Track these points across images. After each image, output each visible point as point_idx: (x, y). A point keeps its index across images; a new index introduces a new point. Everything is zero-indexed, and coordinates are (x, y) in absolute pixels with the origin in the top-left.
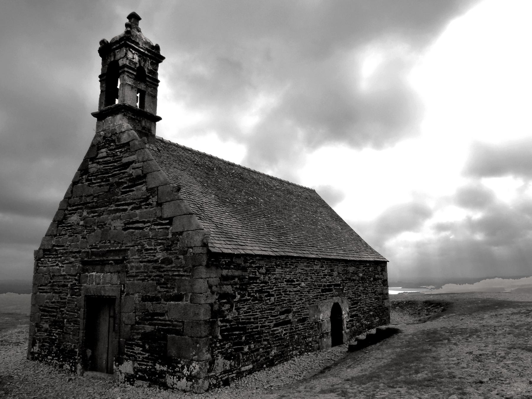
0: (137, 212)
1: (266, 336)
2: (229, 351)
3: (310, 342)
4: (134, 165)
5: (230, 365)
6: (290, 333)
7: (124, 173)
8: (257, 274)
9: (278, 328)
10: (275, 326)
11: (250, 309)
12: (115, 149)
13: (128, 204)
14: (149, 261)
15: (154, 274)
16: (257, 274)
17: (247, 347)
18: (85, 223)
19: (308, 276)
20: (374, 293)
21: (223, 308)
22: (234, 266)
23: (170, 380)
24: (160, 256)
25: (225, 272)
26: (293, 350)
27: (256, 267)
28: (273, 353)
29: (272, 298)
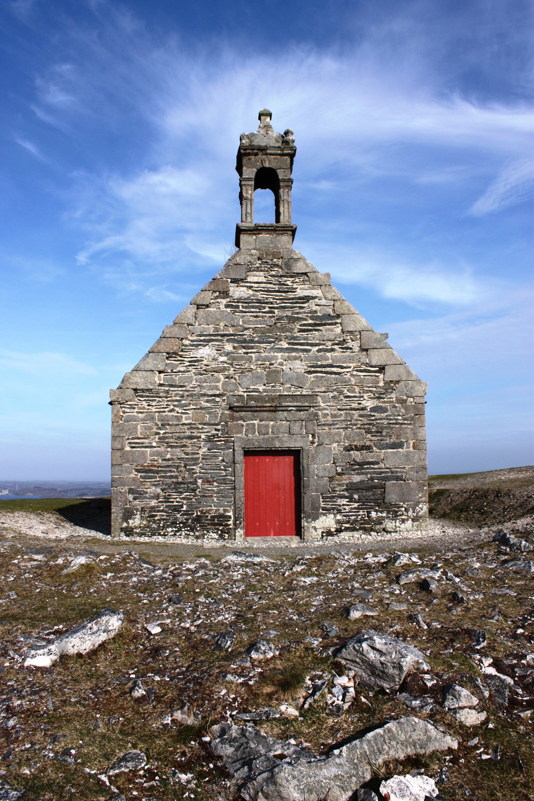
4: (317, 300)
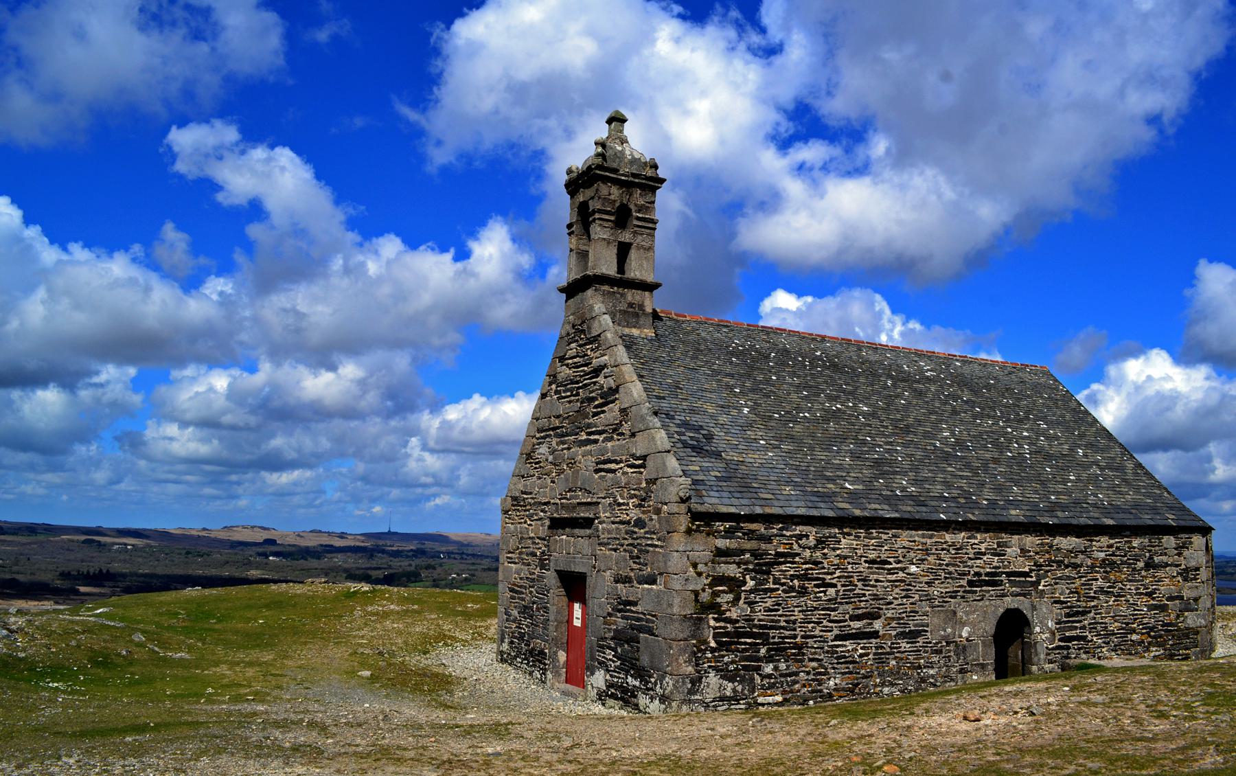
0: (609, 444)
1: (815, 653)
2: (731, 667)
3: (933, 676)
5: (734, 690)
6: (875, 654)
7: (595, 383)
8: (795, 546)
9: (847, 643)
10: (837, 638)
11: (779, 605)
12: (585, 344)
13: (600, 433)
14: (622, 522)
15: (626, 542)
16: (795, 546)
17: (771, 666)
18: (555, 458)
19: (928, 555)
20: (1149, 595)
21: (719, 600)
22: (744, 534)
23: (643, 700)
24: (634, 514)
25: (722, 543)
26: (883, 684)
27: (791, 536)
28: (832, 683)
29: (831, 591)
